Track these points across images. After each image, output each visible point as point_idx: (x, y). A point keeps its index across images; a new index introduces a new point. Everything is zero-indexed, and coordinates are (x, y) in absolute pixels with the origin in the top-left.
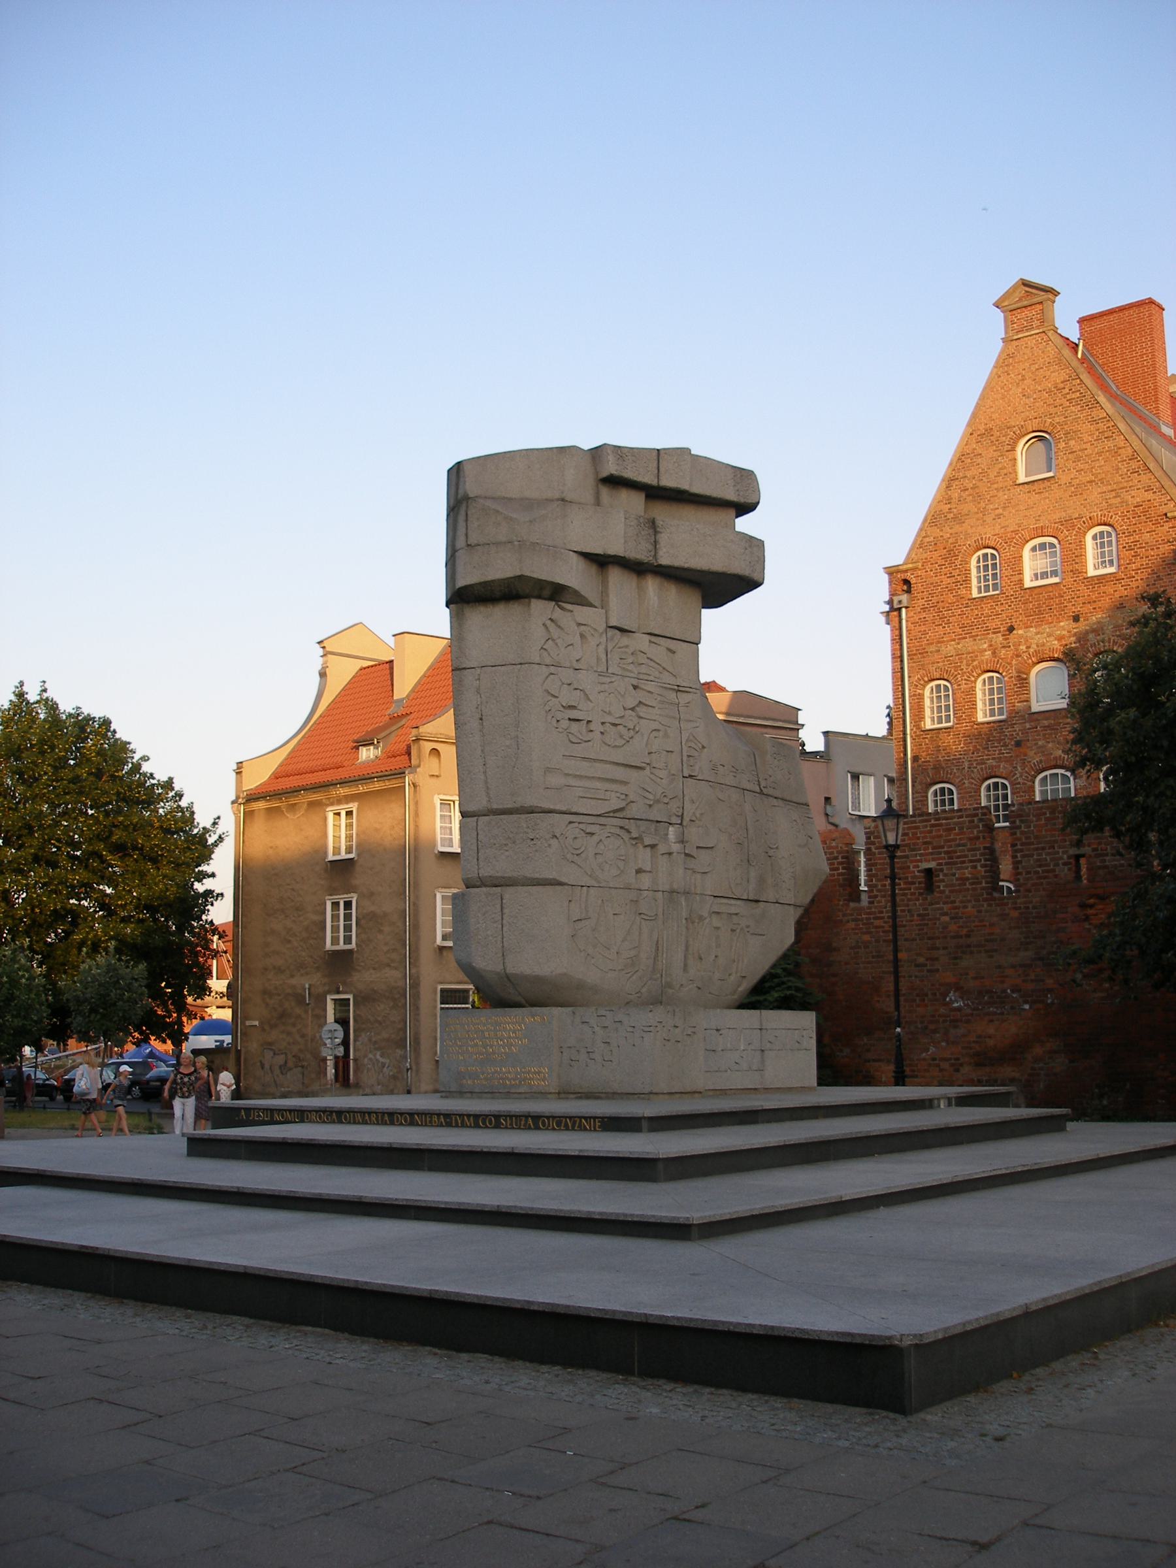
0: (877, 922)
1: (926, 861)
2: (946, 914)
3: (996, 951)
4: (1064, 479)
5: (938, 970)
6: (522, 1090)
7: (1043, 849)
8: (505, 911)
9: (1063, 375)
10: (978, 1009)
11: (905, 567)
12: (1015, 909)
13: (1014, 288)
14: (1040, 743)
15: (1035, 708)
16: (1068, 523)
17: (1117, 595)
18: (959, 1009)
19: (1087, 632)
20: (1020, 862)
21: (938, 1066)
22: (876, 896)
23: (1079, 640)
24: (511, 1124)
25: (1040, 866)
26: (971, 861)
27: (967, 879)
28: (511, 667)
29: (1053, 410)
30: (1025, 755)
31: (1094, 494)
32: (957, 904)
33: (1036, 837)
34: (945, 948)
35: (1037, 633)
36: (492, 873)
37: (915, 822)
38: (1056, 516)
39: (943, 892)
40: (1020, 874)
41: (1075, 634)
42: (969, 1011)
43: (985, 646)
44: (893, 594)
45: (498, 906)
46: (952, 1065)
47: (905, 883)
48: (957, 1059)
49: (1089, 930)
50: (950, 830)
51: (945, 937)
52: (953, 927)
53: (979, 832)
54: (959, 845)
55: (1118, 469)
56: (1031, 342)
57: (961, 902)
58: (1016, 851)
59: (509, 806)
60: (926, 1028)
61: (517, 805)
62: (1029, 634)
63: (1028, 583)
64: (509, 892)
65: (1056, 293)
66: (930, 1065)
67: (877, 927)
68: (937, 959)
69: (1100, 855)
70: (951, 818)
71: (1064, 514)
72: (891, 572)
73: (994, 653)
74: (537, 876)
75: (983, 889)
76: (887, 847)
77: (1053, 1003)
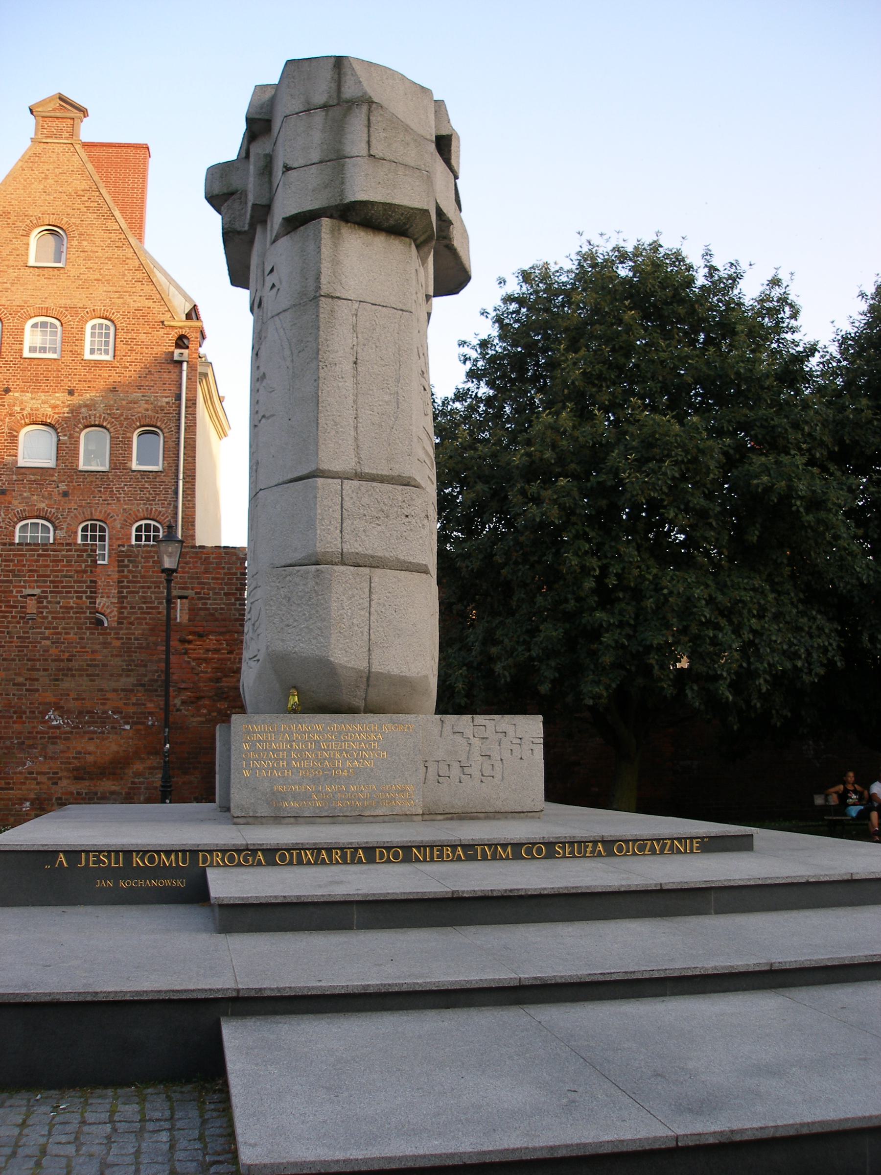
1: (30, 587)
2: (47, 638)
3: (98, 675)
4: (73, 272)
5: (38, 690)
6: (379, 812)
7: (149, 588)
8: (373, 597)
9: (84, 185)
10: (78, 728)
12: (117, 639)
13: (50, 99)
14: (25, 494)
15: (21, 463)
16: (73, 310)
17: (111, 380)
18: (58, 727)
19: (80, 406)
20: (126, 597)
21: (36, 779)
23: (71, 411)
24: (572, 852)
25: (145, 603)
26: (76, 592)
27: (72, 608)
30: (10, 503)
31: (100, 291)
32: (59, 630)
33: (142, 577)
34: (45, 670)
35: (32, 399)
36: (360, 550)
37: (22, 550)
38: (63, 302)
39: (47, 617)
40: (125, 608)
41: (69, 406)
45: (367, 590)
46: (49, 779)
47: (6, 606)
48: (56, 773)
49: (189, 663)
52: (53, 651)
53: (86, 566)
54: (66, 576)
55: (124, 275)
56: (58, 149)
57: (64, 628)
58: (122, 587)
59: (385, 473)
60: (23, 743)
61: (395, 473)
62: (24, 398)
63: (26, 354)
64: (378, 574)
65: (84, 112)
66: (26, 778)
68: (37, 680)
69: (202, 598)
74: (411, 559)
75: (86, 618)
76: (164, 571)
77: (153, 725)
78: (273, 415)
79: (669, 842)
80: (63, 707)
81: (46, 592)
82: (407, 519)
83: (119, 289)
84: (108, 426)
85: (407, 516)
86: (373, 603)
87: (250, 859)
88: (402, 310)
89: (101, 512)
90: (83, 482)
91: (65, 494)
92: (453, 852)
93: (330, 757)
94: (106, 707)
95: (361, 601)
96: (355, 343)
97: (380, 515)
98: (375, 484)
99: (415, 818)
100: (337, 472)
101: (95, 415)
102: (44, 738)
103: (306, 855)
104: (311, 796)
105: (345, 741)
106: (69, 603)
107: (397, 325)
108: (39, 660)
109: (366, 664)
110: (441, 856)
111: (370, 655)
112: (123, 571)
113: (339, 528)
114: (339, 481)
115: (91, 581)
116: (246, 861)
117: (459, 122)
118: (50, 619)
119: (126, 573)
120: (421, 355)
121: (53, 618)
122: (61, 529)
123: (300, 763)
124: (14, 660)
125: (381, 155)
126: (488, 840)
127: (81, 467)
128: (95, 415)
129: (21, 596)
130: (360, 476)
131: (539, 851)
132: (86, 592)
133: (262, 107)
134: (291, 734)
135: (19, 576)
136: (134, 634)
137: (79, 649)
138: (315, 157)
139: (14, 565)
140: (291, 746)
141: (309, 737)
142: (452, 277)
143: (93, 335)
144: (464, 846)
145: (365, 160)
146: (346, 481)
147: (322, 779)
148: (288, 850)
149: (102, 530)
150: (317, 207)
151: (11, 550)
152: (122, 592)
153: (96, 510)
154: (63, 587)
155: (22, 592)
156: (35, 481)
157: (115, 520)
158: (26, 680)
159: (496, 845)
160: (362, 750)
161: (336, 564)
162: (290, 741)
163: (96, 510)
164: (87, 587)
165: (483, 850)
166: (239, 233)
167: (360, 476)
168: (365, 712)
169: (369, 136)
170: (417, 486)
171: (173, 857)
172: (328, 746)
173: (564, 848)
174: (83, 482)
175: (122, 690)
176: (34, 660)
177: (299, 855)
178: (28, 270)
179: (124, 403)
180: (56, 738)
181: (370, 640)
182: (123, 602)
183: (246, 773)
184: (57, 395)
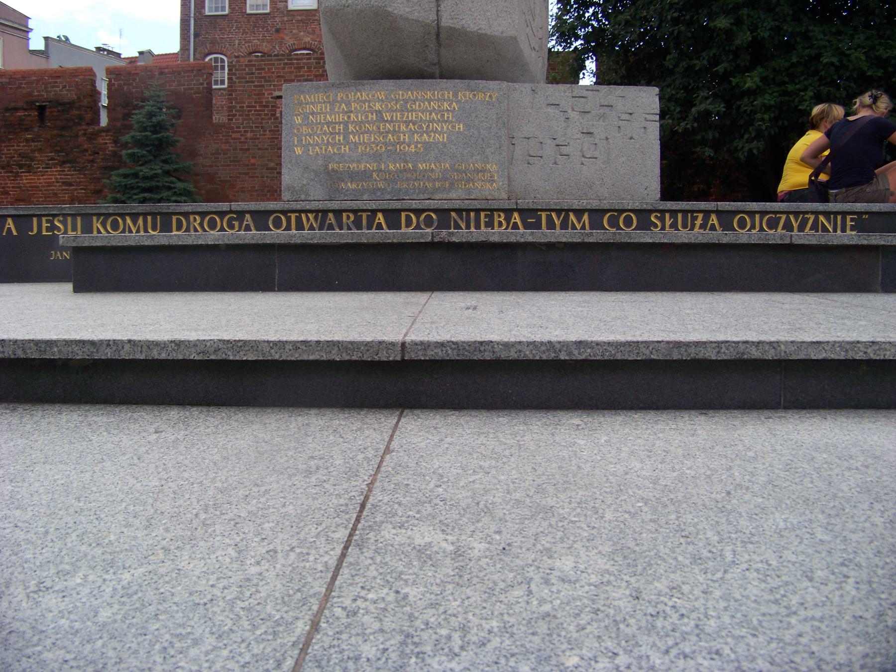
0: (234, 135)
22: (235, 115)
47: (260, 106)
70: (302, 59)
79: (812, 217)
87: (236, 224)
93: (394, 130)
103: (308, 219)
104: (371, 175)
123: (359, 138)
124: (266, 149)
126: (556, 204)
134: (348, 104)
135: (269, 81)
139: (266, 73)
140: (349, 117)
141: (369, 106)
144: (521, 211)
151: (262, 61)
162: (346, 112)
165: (549, 218)
168: (442, 77)
171: (140, 221)
172: (392, 117)
183: (298, 151)
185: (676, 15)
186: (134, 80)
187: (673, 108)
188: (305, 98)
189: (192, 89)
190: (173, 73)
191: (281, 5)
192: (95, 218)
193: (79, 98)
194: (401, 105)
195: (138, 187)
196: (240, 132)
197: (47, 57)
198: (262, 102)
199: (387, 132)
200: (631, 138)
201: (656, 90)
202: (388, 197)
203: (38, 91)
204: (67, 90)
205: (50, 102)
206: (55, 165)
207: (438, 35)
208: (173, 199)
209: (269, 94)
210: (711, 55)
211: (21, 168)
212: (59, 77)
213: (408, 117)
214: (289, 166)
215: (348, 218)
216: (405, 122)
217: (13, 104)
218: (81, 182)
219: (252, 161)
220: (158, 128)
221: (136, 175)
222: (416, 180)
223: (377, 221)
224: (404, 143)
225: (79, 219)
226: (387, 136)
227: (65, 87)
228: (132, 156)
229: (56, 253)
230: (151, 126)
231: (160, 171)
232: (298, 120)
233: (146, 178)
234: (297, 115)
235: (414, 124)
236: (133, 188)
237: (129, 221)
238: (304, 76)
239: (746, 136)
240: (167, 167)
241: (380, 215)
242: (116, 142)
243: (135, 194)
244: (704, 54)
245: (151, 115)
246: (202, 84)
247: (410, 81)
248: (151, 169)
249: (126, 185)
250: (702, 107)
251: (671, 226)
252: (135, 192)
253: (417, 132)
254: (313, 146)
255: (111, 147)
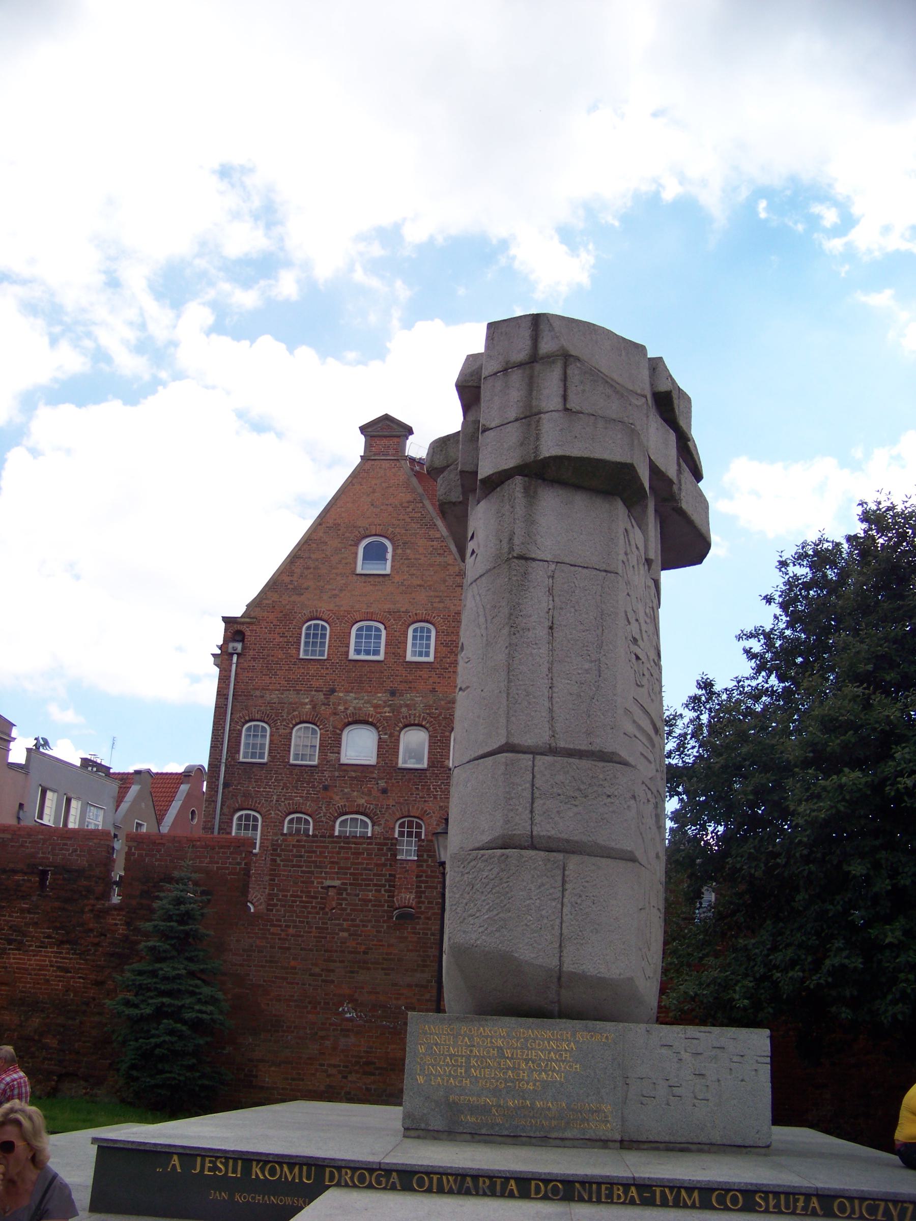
0: (273, 930)
2: (343, 930)
3: (393, 969)
5: (333, 982)
6: (568, 1134)
8: (567, 886)
9: (409, 497)
11: (243, 620)
12: (414, 933)
18: (351, 1020)
20: (424, 892)
21: (326, 1071)
24: (777, 1206)
26: (375, 885)
27: (370, 901)
28: (595, 572)
29: (395, 522)
30: (331, 798)
32: (358, 922)
35: (355, 699)
37: (324, 842)
38: (387, 607)
39: (345, 909)
40: (423, 903)
42: (361, 1022)
43: (307, 700)
44: (226, 640)
45: (560, 878)
48: (346, 1067)
50: (357, 854)
51: (342, 952)
53: (387, 860)
54: (365, 869)
56: (386, 464)
57: (361, 921)
61: (595, 748)
64: (573, 862)
67: (273, 934)
68: (333, 971)
70: (361, 844)
71: (392, 606)
72: (228, 621)
73: (314, 707)
74: (613, 845)
75: (384, 911)
78: (468, 687)
79: (882, 1204)
80: (357, 1000)
81: (345, 884)
82: (609, 800)
83: (440, 594)
84: (428, 725)
85: (609, 796)
86: (567, 893)
87: (383, 1180)
88: (606, 571)
89: (418, 809)
90: (402, 779)
91: (384, 791)
92: (626, 1192)
94: (400, 1002)
95: (551, 891)
96: (551, 607)
97: (577, 794)
98: (571, 760)
99: (611, 1144)
100: (529, 747)
101: (415, 714)
102: (337, 1030)
105: (532, 1049)
106: (368, 896)
107: (599, 587)
108: (336, 951)
109: (556, 962)
110: (610, 1196)
111: (561, 952)
112: (422, 866)
113: (529, 809)
114: (531, 756)
115: (390, 875)
116: (379, 1183)
117: (684, 375)
118: (348, 911)
119: (425, 868)
120: (632, 621)
121: (351, 910)
122: (379, 825)
123: (480, 1072)
124: (311, 950)
125: (578, 408)
127: (401, 764)
128: (415, 714)
129: (322, 888)
130: (552, 751)
131: (735, 1200)
132: (385, 886)
133: (471, 375)
135: (320, 867)
136: (430, 929)
137: (375, 943)
138: (512, 414)
139: (317, 857)
140: (471, 1051)
142: (686, 543)
143: (414, 638)
145: (561, 414)
146: (538, 757)
147: (504, 1092)
148: (428, 1174)
149: (419, 826)
150: (511, 466)
151: (313, 842)
152: (421, 887)
153: (413, 806)
154: (362, 880)
155: (322, 883)
156: (355, 778)
157: (431, 817)
158: (322, 970)
159: (679, 1188)
160: (551, 1060)
161: (525, 848)
162: (469, 1046)
163: (413, 806)
164: (386, 880)
165: (663, 1194)
166: (454, 504)
167: (552, 751)
168: (560, 1017)
169: (565, 390)
170: (625, 764)
171: (296, 1170)
173: (766, 1200)
174: (402, 779)
175: (417, 986)
176: (331, 951)
177: (440, 1181)
178: (355, 577)
179: (443, 703)
180: (348, 1030)
181: (561, 934)
182: (421, 897)
184: (380, 695)
185: (805, 852)
186: (159, 851)
187: (803, 957)
188: (429, 1028)
189: (227, 868)
190: (206, 846)
191: (332, 756)
192: (254, 1163)
193: (90, 865)
194: (521, 1043)
195: (156, 989)
196: (280, 926)
197: (27, 774)
198: (309, 892)
199: (508, 1069)
200: (742, 1080)
201: (767, 1032)
202: (506, 1133)
203: (43, 853)
204: (77, 855)
205: (55, 867)
206: (51, 945)
207: (559, 978)
208: (197, 1007)
209: (318, 883)
210: (846, 899)
211: (10, 944)
212: (69, 838)
213: (527, 1055)
214: (411, 1094)
215: (484, 1182)
216: (525, 1060)
217: (11, 865)
218: (80, 969)
219: (293, 963)
220: (185, 918)
221: (154, 974)
222: (533, 1117)
223: (509, 1187)
224: (523, 1080)
225: (240, 1162)
226: (506, 1073)
227: (76, 851)
228: (152, 949)
229: (215, 1193)
230: (178, 915)
231: (184, 972)
232: (422, 1050)
233: (166, 979)
234: (421, 1044)
235: (533, 1062)
236: (149, 990)
237: (286, 1168)
238: (362, 864)
239: (890, 997)
240: (193, 967)
241: (512, 1182)
242: (128, 924)
243: (152, 998)
244: (838, 897)
245: (179, 901)
246: (239, 864)
247: (531, 1020)
248: (174, 968)
249: (140, 985)
250: (836, 961)
251: (774, 1207)
252: (152, 994)
253: (535, 1070)
254: (436, 1076)
255: (122, 930)
